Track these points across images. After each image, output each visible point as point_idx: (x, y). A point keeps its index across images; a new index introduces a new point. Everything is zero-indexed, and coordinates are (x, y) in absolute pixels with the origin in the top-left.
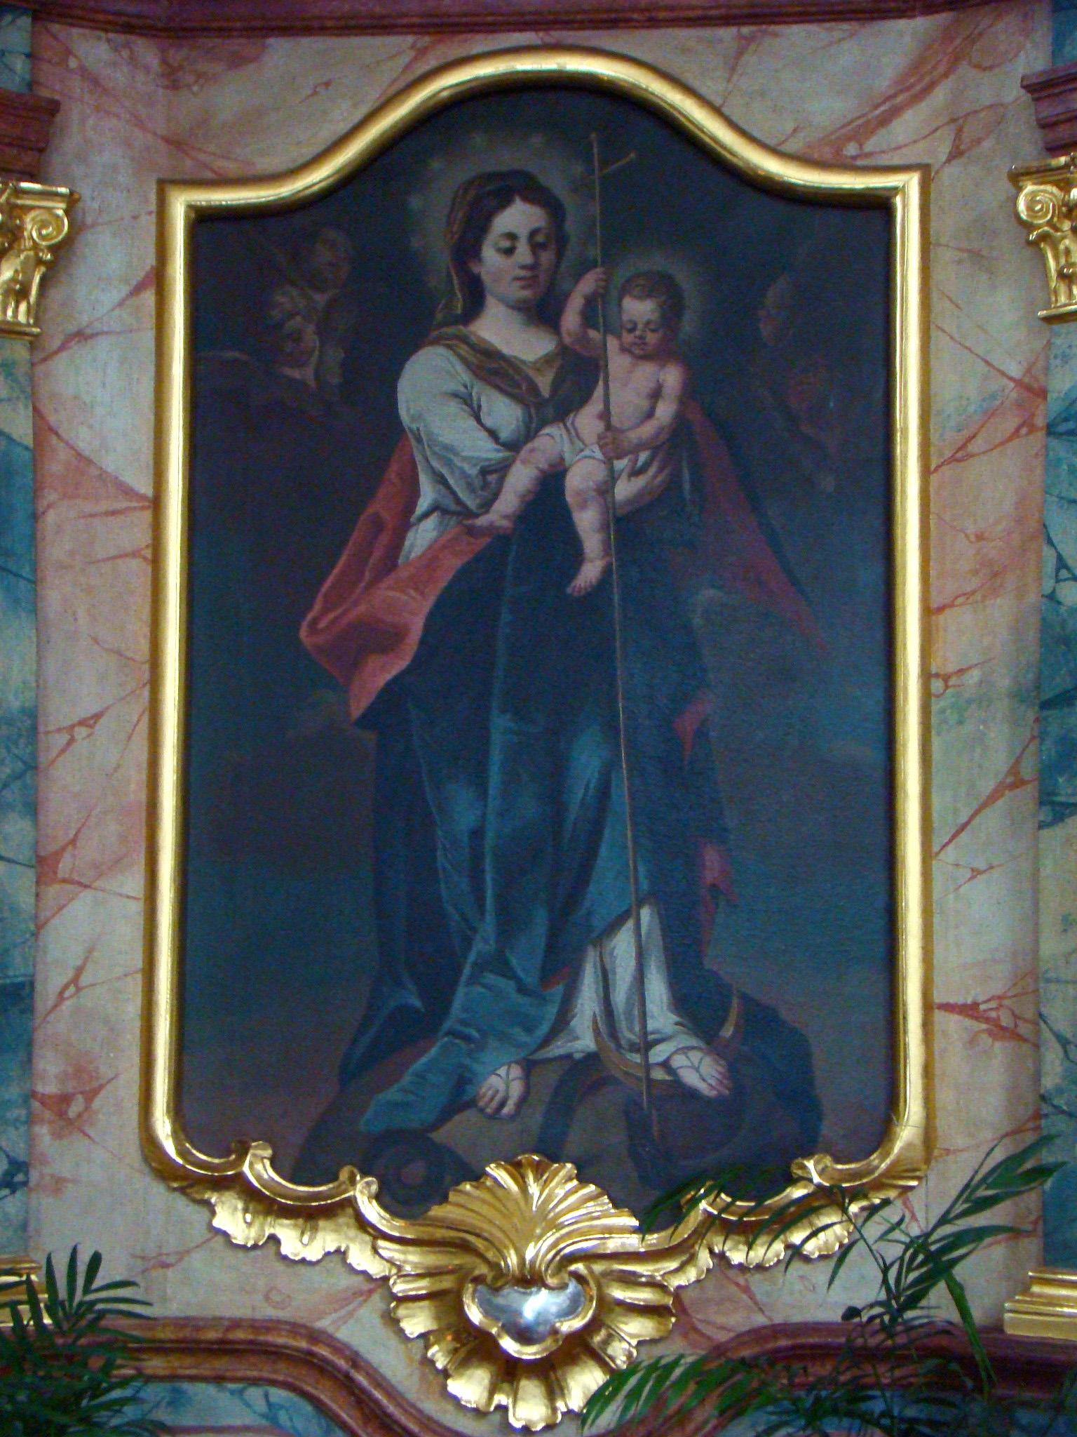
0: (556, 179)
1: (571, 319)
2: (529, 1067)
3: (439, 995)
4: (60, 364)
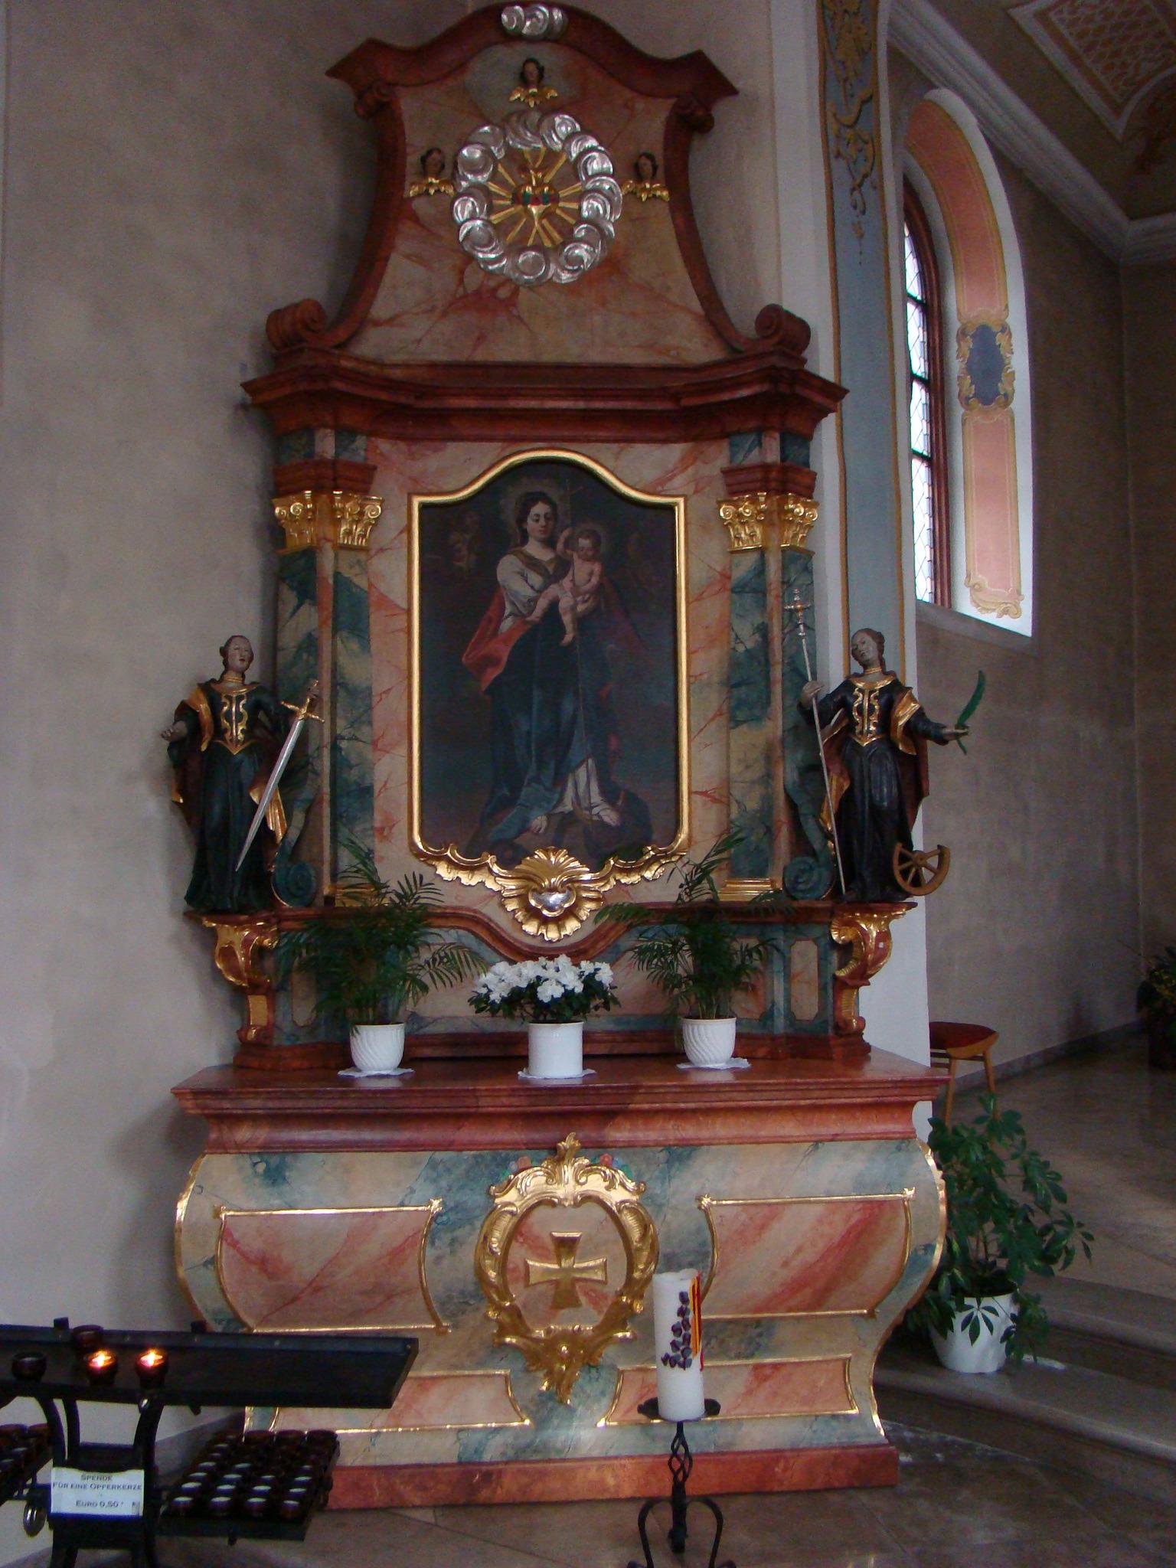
0: (554, 494)
1: (560, 546)
2: (549, 816)
3: (516, 790)
4: (374, 561)
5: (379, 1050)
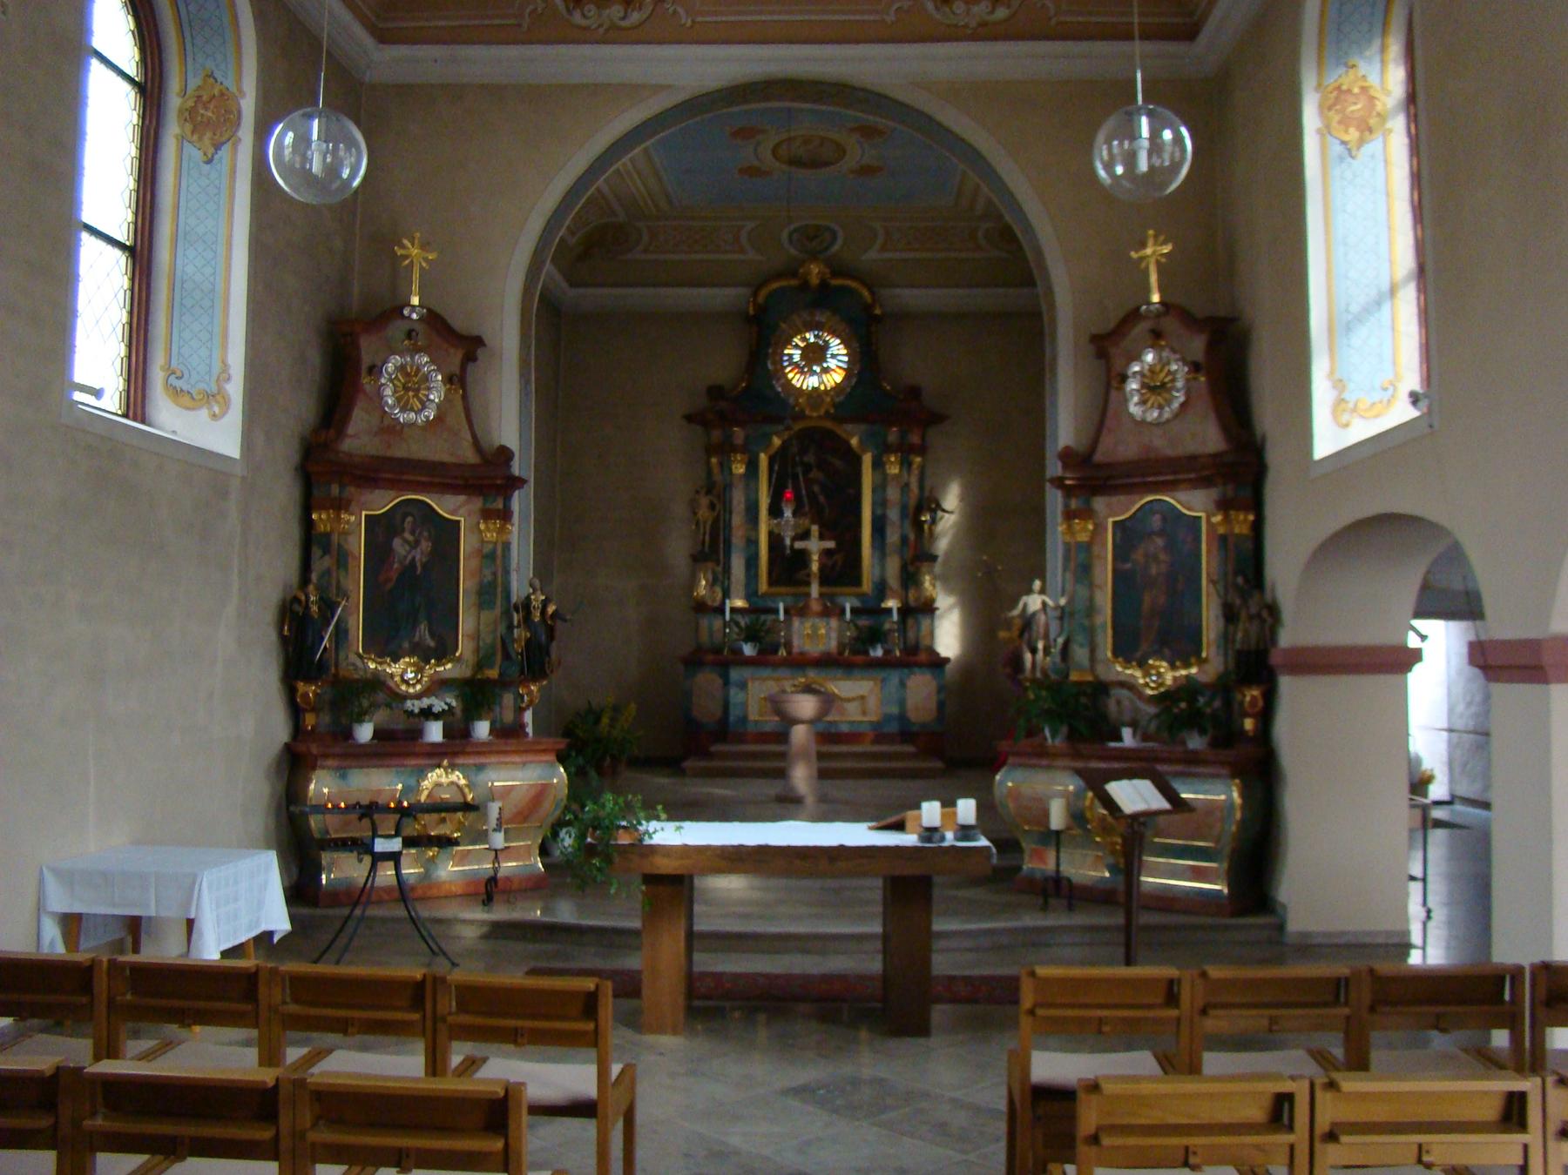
5: (365, 732)
